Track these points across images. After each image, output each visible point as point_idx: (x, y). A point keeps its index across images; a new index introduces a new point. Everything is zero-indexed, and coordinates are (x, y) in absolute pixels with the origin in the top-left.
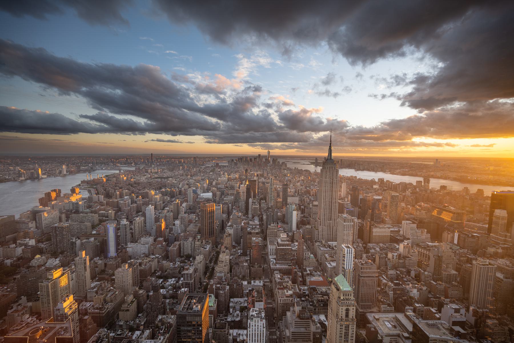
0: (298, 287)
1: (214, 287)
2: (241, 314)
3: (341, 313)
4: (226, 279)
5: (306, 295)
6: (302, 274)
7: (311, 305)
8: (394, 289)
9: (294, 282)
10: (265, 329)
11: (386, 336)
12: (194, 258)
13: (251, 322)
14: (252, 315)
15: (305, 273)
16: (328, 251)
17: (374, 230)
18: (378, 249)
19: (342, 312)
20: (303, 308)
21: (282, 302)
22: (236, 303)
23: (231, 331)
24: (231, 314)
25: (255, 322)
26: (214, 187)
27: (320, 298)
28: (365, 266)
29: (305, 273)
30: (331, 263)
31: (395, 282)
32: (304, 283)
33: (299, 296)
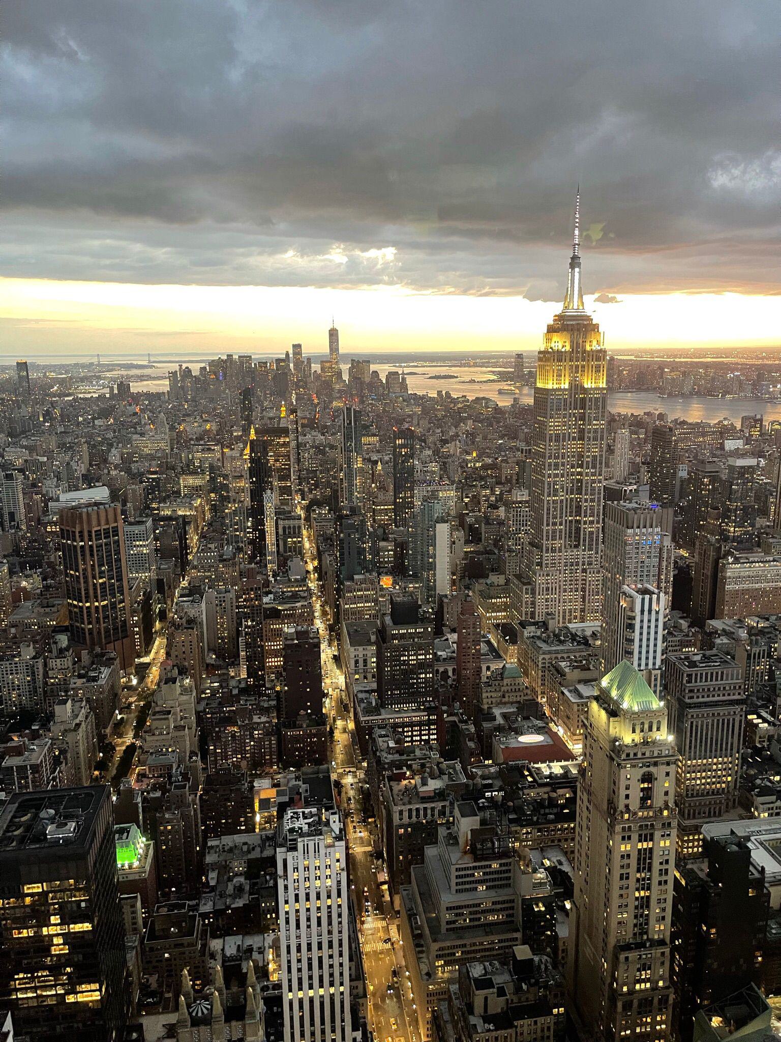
2: (253, 886)
3: (623, 792)
14: (292, 830)
16: (569, 651)
17: (733, 569)
18: (743, 634)
19: (627, 788)
20: (483, 822)
21: (406, 820)
22: (231, 850)
23: (216, 944)
24: (213, 889)
28: (702, 669)
29: (486, 725)
30: (580, 687)
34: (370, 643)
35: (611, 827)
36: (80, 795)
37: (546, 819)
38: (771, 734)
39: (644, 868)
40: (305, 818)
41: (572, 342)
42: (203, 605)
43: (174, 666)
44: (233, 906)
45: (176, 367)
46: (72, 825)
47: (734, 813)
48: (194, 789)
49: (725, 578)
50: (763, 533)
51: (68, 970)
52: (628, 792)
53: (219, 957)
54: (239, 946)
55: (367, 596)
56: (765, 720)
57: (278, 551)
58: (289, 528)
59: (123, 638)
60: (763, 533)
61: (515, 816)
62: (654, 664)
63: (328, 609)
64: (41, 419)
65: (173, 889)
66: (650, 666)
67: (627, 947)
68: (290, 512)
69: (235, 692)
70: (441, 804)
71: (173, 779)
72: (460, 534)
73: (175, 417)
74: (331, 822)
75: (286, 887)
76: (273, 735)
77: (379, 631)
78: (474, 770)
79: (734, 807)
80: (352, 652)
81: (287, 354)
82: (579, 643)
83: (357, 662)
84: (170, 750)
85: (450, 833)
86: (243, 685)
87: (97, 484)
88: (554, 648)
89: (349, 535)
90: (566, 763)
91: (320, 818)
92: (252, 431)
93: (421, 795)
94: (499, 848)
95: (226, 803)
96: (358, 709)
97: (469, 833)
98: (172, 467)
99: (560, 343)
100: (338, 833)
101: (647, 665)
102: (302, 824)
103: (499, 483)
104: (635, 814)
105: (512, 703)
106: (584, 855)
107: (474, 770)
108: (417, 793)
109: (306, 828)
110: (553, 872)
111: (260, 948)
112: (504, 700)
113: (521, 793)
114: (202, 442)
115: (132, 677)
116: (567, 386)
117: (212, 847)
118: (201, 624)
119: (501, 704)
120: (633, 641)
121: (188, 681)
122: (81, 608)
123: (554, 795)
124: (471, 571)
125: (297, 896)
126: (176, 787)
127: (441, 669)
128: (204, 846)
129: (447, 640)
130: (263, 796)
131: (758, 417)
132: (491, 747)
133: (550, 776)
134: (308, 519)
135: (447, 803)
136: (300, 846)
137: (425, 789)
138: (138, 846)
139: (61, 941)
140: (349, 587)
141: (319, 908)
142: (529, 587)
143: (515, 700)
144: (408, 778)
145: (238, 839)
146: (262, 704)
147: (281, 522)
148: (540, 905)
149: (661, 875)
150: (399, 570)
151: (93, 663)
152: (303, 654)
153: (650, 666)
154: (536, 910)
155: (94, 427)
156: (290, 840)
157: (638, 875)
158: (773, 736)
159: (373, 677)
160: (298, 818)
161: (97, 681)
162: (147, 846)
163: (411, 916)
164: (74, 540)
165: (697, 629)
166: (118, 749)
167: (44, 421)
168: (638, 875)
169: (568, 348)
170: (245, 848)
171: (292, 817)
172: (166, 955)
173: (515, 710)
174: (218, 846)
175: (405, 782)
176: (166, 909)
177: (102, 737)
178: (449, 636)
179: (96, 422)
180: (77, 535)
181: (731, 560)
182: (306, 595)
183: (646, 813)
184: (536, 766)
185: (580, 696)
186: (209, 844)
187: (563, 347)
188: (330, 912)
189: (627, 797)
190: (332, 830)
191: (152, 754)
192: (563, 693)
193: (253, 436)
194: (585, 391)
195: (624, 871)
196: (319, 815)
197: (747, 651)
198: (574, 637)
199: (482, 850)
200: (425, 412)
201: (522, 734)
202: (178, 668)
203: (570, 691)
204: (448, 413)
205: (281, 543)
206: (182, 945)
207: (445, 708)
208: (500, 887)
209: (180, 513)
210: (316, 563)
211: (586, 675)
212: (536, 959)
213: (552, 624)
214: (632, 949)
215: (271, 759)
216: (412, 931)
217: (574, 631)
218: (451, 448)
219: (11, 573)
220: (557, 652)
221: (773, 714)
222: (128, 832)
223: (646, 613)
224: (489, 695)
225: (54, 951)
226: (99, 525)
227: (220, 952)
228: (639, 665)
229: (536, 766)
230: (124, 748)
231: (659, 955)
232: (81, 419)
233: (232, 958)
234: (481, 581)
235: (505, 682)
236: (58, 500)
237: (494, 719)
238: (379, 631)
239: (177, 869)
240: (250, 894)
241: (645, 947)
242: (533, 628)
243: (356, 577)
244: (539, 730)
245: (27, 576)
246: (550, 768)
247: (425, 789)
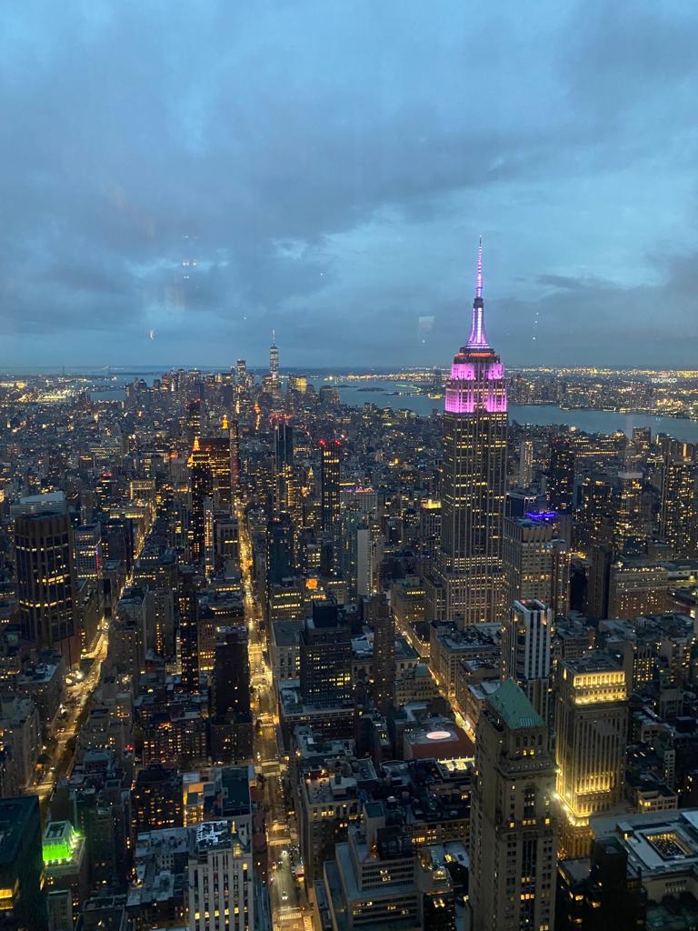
0: (376, 766)
1: (73, 796)
5: (404, 789)
7: (418, 817)
8: (677, 741)
10: (250, 886)
11: (655, 878)
14: (203, 843)
15: (398, 722)
16: (475, 650)
20: (389, 822)
22: (159, 845)
25: (216, 864)
27: (449, 793)
29: (398, 722)
30: (486, 685)
31: (682, 719)
32: (395, 753)
34: (293, 643)
36: (10, 806)
37: (449, 815)
41: (476, 372)
42: (143, 605)
43: (113, 665)
44: (158, 899)
45: (130, 379)
48: (126, 785)
58: (227, 531)
59: (62, 639)
62: (544, 673)
64: (9, 426)
65: (104, 882)
66: (540, 675)
68: (228, 516)
69: (170, 688)
75: (197, 897)
76: (203, 731)
77: (303, 633)
84: (106, 746)
86: (178, 681)
88: (464, 647)
90: (470, 759)
92: (196, 443)
94: (403, 847)
98: (124, 472)
101: (537, 674)
104: (521, 822)
105: (422, 701)
106: (476, 858)
107: (385, 767)
109: (216, 840)
110: (453, 868)
115: (77, 672)
117: (142, 841)
119: (411, 702)
121: (126, 679)
124: (390, 571)
125: (207, 905)
127: (359, 668)
128: (135, 841)
129: (365, 639)
130: (192, 790)
134: (245, 521)
135: (359, 801)
136: (210, 859)
140: (277, 589)
141: (227, 917)
144: (324, 776)
145: (167, 833)
147: (219, 526)
148: (441, 901)
151: (40, 661)
153: (540, 675)
154: (436, 906)
155: (56, 433)
156: (201, 853)
158: (656, 732)
159: (297, 674)
160: (209, 831)
165: (592, 628)
166: (60, 742)
167: (13, 428)
170: (172, 842)
173: (425, 708)
176: (94, 905)
180: (30, 541)
184: (442, 762)
186: (140, 838)
190: (240, 842)
191: (89, 750)
197: (634, 650)
198: (480, 635)
200: (356, 419)
201: (431, 731)
203: (475, 688)
207: (360, 706)
209: (129, 516)
210: (251, 563)
215: (201, 753)
217: (481, 630)
218: (379, 456)
220: (465, 651)
222: (62, 829)
223: (535, 627)
224: (402, 692)
226: (51, 533)
229: (442, 762)
230: (65, 741)
234: (398, 581)
235: (417, 680)
236: (18, 503)
238: (303, 633)
242: (443, 628)
243: (284, 580)
244: (446, 727)
246: (454, 764)
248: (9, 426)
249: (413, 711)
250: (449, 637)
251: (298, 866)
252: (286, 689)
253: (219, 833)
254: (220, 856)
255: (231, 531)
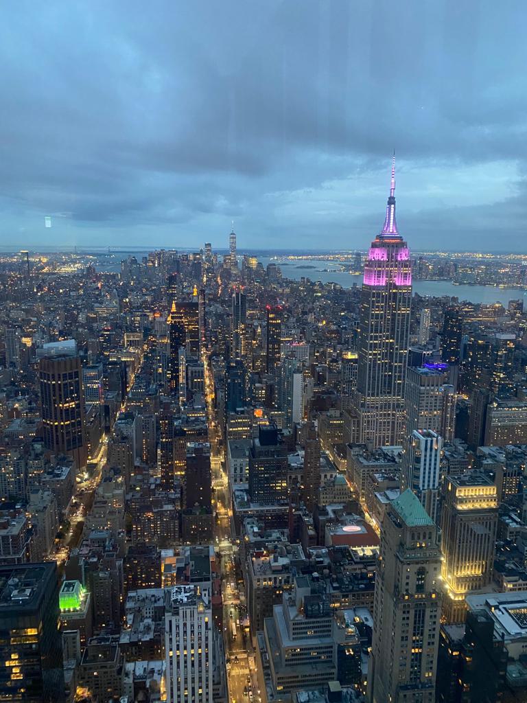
0: (304, 549)
1: (82, 563)
3: (404, 581)
4: (114, 547)
5: (325, 567)
6: (316, 520)
7: (335, 588)
9: (296, 536)
11: (513, 641)
12: (26, 503)
13: (174, 619)
14: (176, 601)
18: (502, 458)
19: (408, 578)
20: (313, 591)
23: (129, 666)
25: (185, 616)
26: (82, 326)
27: (358, 572)
29: (321, 518)
30: (388, 492)
32: (319, 540)
33: (307, 569)
35: (396, 604)
38: (518, 530)
39: (418, 634)
40: (185, 592)
42: (134, 425)
44: (143, 640)
46: (28, 592)
47: (489, 588)
49: (491, 418)
50: (519, 386)
51: (22, 690)
52: (407, 581)
53: (131, 676)
54: (145, 668)
55: (244, 422)
56: (514, 521)
57: (187, 388)
58: (196, 372)
60: (519, 386)
61: (337, 585)
62: (434, 485)
63: (219, 428)
64: (35, 290)
65: (104, 625)
66: (431, 487)
67: (405, 688)
68: (196, 361)
69: (153, 487)
70: (286, 575)
71: (107, 548)
72: (310, 381)
73: (123, 292)
74: (203, 595)
75: (171, 639)
78: (311, 551)
79: (490, 583)
80: (232, 462)
81: (201, 250)
82: (389, 460)
83: (236, 469)
85: (291, 598)
86: (158, 482)
87: (69, 337)
88: (372, 464)
89: (234, 380)
90: (375, 547)
91: (196, 593)
92: (174, 306)
93: (273, 569)
95: (142, 566)
96: (235, 503)
97: (303, 598)
99: (380, 255)
100: (207, 603)
101: (429, 486)
102: (183, 597)
103: (339, 343)
105: (340, 503)
106: (378, 620)
107: (311, 551)
108: (271, 567)
110: (361, 627)
111: (159, 671)
112: (335, 500)
113: (342, 568)
114: (140, 310)
115: (84, 473)
116: (384, 284)
117: (131, 597)
118: (132, 438)
119: (331, 503)
120: (419, 469)
121: (120, 479)
122: (51, 425)
123: (364, 571)
124: (318, 405)
125: (178, 646)
126: (108, 556)
127: (293, 476)
129: (298, 455)
131: (520, 301)
132: (324, 537)
133: (362, 558)
135: (291, 575)
136: (181, 612)
137: (276, 564)
138: (80, 596)
139: (18, 671)
141: (193, 655)
142: (356, 420)
143: (342, 500)
144: (265, 556)
146: (170, 496)
147: (190, 368)
148: (351, 650)
149: (434, 635)
150: (268, 405)
152: (199, 469)
153: (431, 487)
154: (347, 654)
155: (70, 296)
156: (174, 608)
157: (414, 638)
159: (247, 479)
160: (180, 593)
161: (59, 477)
162: (87, 596)
163: (263, 653)
164: (49, 380)
165: (471, 452)
168: (414, 638)
169: (385, 258)
170: (153, 599)
171: (177, 591)
172: (95, 673)
173: (342, 508)
174: (134, 597)
175: (263, 558)
177: (61, 515)
178: (299, 453)
179: (71, 293)
181: (495, 405)
182: (204, 419)
183: (420, 596)
185: (388, 498)
186: (129, 595)
187: (382, 257)
188: (201, 658)
189: (407, 584)
190: (203, 602)
191: (93, 530)
192: (376, 496)
193: (174, 309)
194: (396, 287)
195: (404, 635)
196: (195, 590)
198: (385, 456)
199: (312, 611)
201: (346, 525)
202: (114, 471)
203: (381, 495)
204: (305, 292)
205: (190, 382)
206: (106, 667)
208: (324, 636)
209: (123, 359)
210: (213, 396)
211: (392, 484)
212: (345, 690)
213: (370, 446)
214: (409, 689)
216: (263, 664)
217: (386, 452)
218: (310, 318)
219: (8, 397)
220: (373, 466)
221: (520, 516)
223: (428, 450)
225: (13, 677)
227: (132, 672)
228: (423, 486)
229: (354, 549)
231: (427, 694)
232: (61, 291)
233: (141, 677)
234: (324, 413)
237: (327, 514)
239: (105, 612)
240: (155, 632)
241: (418, 688)
242: (357, 449)
243: (238, 409)
244: (358, 523)
245: (18, 401)
246: (363, 550)
247: (276, 564)
248: (35, 290)
249: (332, 510)
250: (361, 456)
251: (245, 620)
252: (238, 490)
253: (188, 594)
254: (188, 611)
255: (199, 372)
